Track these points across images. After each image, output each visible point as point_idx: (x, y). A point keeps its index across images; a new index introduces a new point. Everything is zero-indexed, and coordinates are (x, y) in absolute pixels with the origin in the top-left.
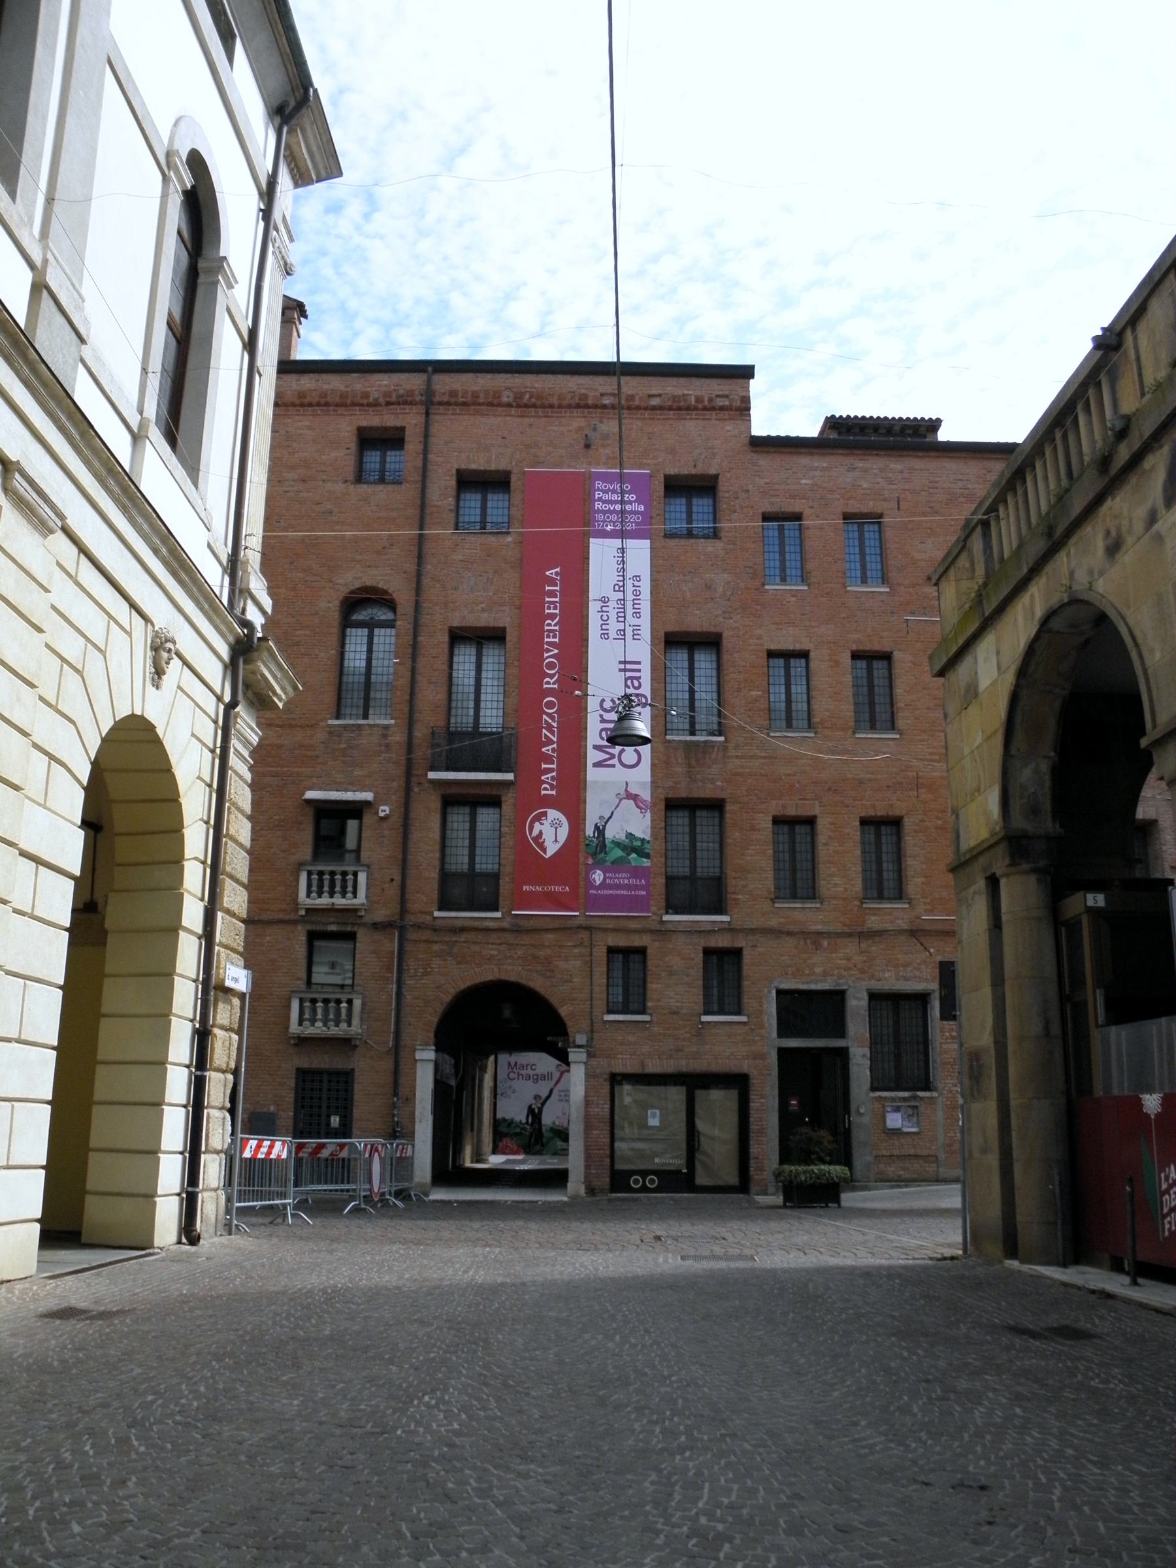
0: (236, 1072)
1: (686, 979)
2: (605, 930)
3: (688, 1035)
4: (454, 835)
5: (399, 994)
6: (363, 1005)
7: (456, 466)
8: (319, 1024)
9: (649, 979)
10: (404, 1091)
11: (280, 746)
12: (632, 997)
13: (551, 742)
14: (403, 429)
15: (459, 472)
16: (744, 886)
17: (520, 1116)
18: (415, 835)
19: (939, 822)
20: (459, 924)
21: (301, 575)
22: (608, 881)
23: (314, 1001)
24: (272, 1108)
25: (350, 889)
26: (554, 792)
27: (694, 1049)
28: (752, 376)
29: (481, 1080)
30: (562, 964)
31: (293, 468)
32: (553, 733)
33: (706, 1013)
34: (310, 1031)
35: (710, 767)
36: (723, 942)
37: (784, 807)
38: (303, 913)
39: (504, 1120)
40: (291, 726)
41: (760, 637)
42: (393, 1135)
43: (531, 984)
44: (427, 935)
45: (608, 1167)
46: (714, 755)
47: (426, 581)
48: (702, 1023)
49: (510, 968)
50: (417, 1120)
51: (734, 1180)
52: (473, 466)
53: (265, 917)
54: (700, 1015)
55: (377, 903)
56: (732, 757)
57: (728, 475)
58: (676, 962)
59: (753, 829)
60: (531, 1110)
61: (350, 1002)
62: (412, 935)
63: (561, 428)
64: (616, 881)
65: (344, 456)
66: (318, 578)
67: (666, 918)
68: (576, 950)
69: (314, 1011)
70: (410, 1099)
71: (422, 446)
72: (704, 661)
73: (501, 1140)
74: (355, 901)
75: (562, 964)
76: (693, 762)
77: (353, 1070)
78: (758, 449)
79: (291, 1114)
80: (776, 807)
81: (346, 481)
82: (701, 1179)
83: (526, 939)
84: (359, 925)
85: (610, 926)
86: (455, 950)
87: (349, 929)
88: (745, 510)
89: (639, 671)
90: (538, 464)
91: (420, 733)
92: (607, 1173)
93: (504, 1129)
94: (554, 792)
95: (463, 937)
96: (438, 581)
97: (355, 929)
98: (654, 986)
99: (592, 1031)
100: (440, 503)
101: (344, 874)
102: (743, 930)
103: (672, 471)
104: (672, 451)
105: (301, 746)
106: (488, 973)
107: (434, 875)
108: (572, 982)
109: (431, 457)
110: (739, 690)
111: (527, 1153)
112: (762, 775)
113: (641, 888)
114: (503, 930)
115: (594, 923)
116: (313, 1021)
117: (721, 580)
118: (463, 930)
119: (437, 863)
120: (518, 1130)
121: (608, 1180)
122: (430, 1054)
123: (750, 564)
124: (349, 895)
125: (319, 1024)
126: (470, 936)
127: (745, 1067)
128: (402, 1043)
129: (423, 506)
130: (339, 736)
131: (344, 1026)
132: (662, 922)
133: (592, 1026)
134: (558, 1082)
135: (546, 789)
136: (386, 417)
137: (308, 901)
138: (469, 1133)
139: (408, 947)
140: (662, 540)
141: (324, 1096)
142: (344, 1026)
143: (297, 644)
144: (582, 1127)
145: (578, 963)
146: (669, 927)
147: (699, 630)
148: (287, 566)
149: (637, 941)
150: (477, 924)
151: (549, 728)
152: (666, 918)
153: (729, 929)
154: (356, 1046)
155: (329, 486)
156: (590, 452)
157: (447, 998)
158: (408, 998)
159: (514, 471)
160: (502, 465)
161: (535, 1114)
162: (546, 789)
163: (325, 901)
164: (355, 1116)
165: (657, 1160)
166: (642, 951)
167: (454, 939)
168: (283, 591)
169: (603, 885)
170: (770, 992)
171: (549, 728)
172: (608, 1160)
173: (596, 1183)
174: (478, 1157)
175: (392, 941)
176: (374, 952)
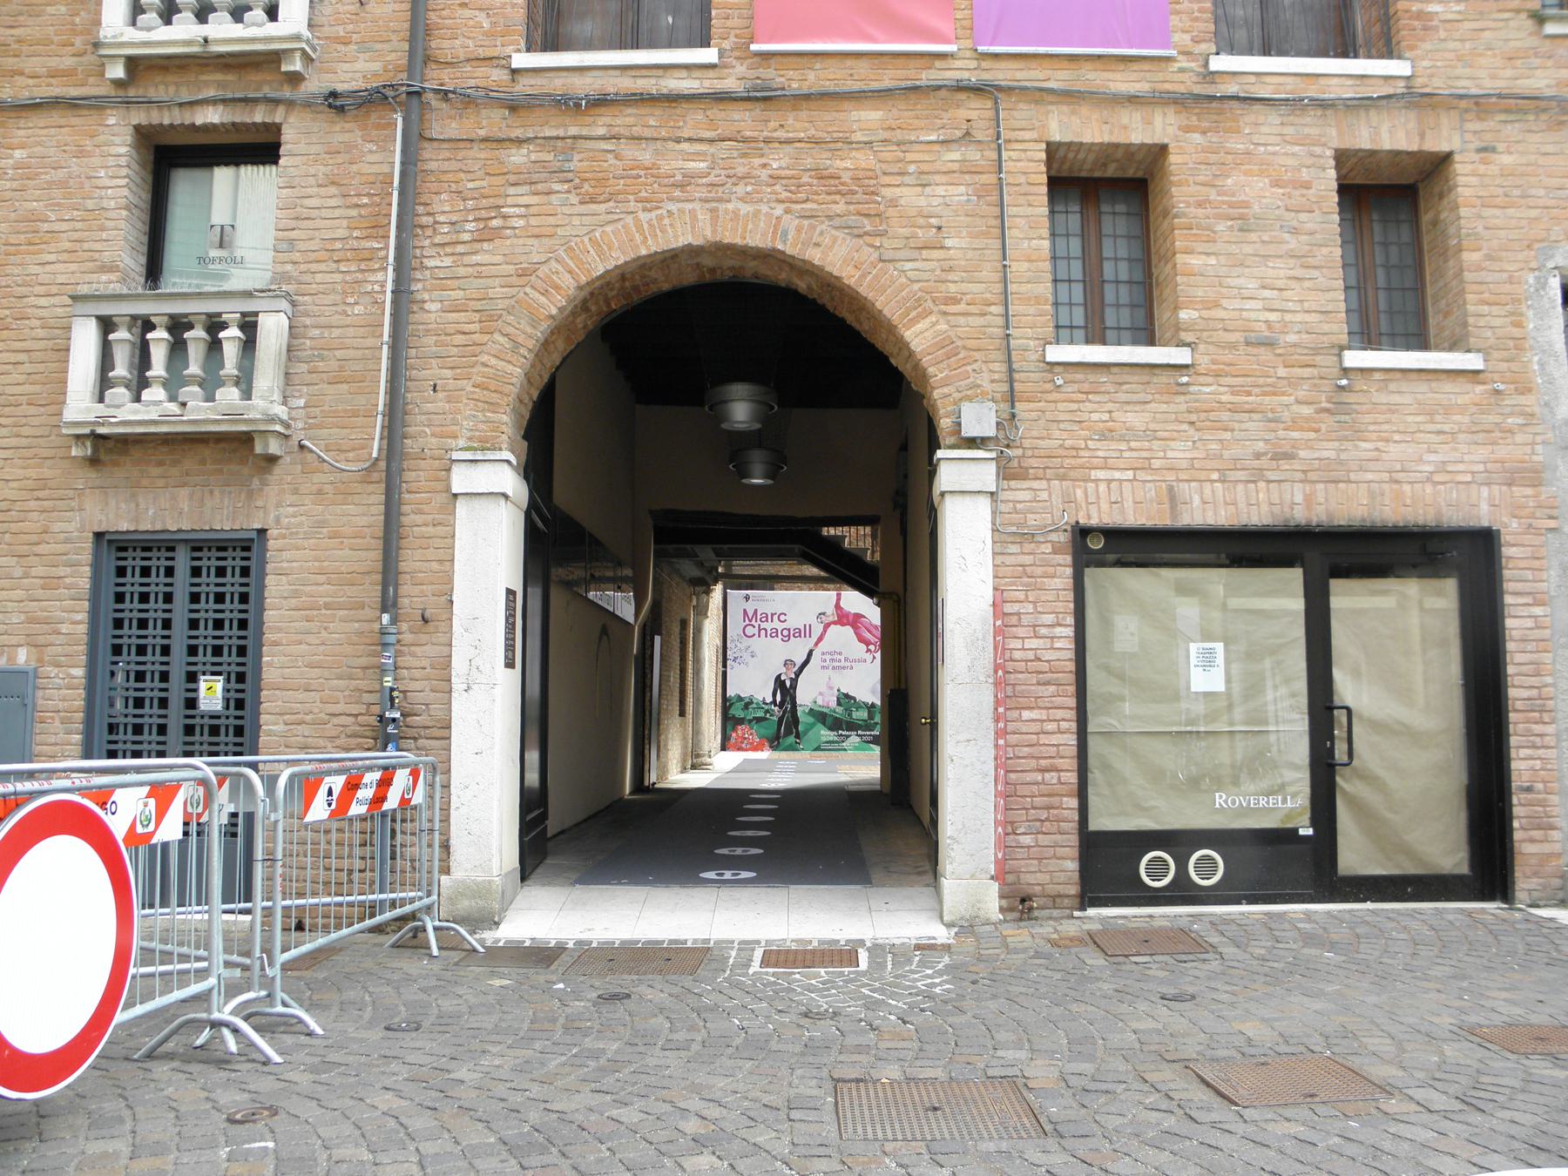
1: (1292, 243)
2: (1040, 95)
3: (1306, 410)
5: (401, 292)
8: (154, 393)
10: (412, 596)
17: (763, 691)
20: (583, 86)
24: (22, 657)
27: (1328, 451)
29: (698, 630)
30: (910, 197)
36: (1392, 135)
38: (118, 71)
39: (740, 698)
42: (384, 733)
43: (815, 256)
44: (493, 121)
45: (1073, 826)
48: (1346, 371)
49: (745, 209)
50: (457, 684)
51: (1447, 851)
54: (1342, 348)
58: (1256, 191)
60: (779, 682)
62: (446, 124)
67: (1220, 63)
69: (143, 358)
70: (434, 620)
73: (734, 729)
74: (271, 29)
75: (910, 197)
77: (262, 532)
79: (79, 672)
82: (1354, 856)
83: (797, 124)
84: (290, 104)
92: (1070, 844)
93: (737, 711)
95: (600, 125)
98: (1195, 261)
99: (1012, 398)
108: (945, 263)
111: (774, 748)
115: (1001, 74)
116: (140, 384)
118: (601, 102)
120: (760, 714)
121: (1072, 866)
126: (624, 120)
131: (229, 395)
132: (1211, 76)
134: (820, 639)
137: (132, 34)
138: (677, 720)
139: (433, 159)
142: (229, 395)
144: (987, 697)
149: (1136, 130)
152: (1220, 63)
153: (1414, 98)
154: (272, 459)
157: (552, 305)
158: (431, 308)
161: (785, 689)
164: (269, 675)
165: (1220, 799)
167: (573, 131)
170: (1542, 285)
172: (1073, 803)
173: (1033, 878)
174: (695, 761)
175: (385, 149)
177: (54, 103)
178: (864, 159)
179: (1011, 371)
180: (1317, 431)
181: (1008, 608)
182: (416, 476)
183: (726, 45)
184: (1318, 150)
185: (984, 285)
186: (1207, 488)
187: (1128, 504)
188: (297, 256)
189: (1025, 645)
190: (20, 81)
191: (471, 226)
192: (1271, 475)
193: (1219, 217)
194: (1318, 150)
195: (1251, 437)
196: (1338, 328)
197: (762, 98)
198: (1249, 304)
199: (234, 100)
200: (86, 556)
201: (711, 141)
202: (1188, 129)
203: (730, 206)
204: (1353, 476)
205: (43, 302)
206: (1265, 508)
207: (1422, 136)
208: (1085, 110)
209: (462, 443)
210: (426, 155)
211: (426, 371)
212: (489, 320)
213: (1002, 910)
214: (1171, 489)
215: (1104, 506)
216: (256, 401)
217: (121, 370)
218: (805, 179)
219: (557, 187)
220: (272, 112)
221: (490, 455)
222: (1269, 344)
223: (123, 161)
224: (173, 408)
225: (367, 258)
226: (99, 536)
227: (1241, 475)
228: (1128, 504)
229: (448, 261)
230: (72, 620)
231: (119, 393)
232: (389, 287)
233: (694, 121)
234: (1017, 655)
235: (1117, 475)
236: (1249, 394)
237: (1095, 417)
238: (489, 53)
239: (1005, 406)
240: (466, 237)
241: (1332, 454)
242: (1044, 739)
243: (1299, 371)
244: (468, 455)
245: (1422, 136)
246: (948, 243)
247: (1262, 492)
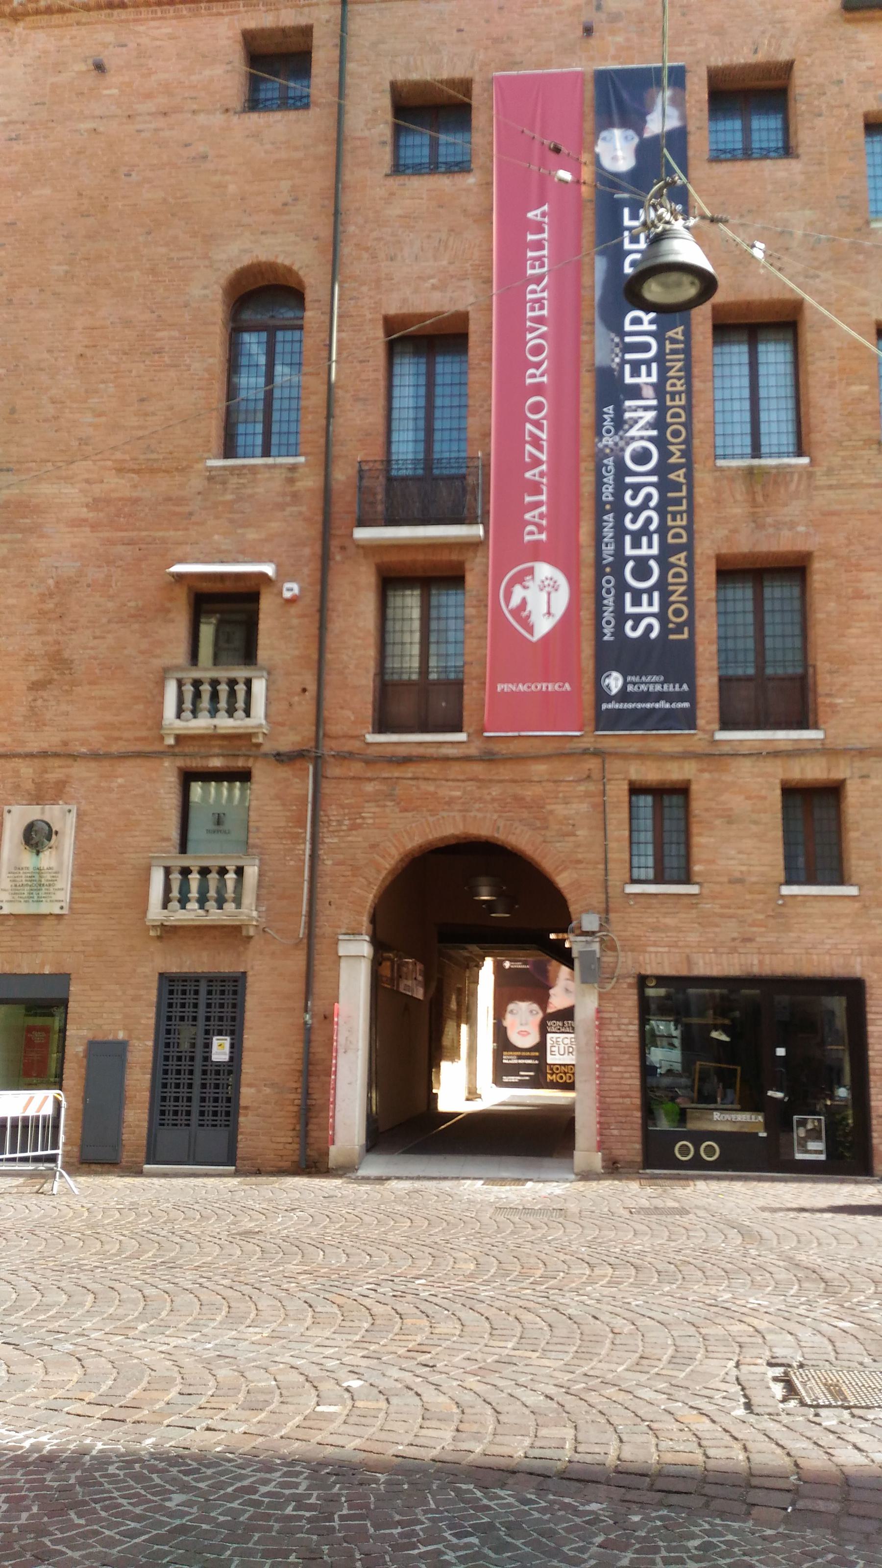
1: (754, 828)
3: (761, 917)
4: (398, 627)
5: (314, 856)
6: (260, 875)
7: (390, 77)
8: (193, 905)
9: (695, 829)
11: (136, 501)
12: (673, 861)
13: (537, 462)
14: (307, 32)
15: (395, 88)
16: (845, 685)
18: (336, 625)
20: (402, 751)
21: (163, 250)
22: (630, 688)
23: (185, 872)
24: (121, 1035)
25: (240, 704)
26: (543, 537)
27: (771, 938)
30: (560, 810)
31: (149, 96)
32: (540, 448)
33: (789, 882)
34: (179, 916)
35: (785, 505)
36: (813, 771)
38: (171, 741)
40: (153, 471)
41: (864, 303)
44: (357, 768)
46: (793, 487)
47: (347, 250)
49: (480, 815)
52: (415, 76)
53: (114, 749)
54: (781, 884)
55: (282, 724)
57: (808, 60)
58: (737, 802)
59: (858, 595)
61: (240, 871)
62: (334, 770)
63: (547, 10)
64: (643, 688)
65: (228, 74)
66: (188, 254)
67: (721, 735)
68: (582, 788)
71: (338, 52)
72: (774, 357)
75: (560, 810)
77: (244, 974)
78: (858, 15)
79: (150, 1043)
81: (227, 110)
83: (505, 772)
84: (256, 757)
85: (632, 750)
86: (398, 791)
87: (240, 763)
88: (836, 112)
90: (514, 65)
91: (343, 474)
94: (543, 537)
95: (410, 771)
96: (367, 249)
97: (250, 763)
99: (607, 911)
100: (366, 133)
101: (232, 683)
102: (845, 751)
103: (719, 60)
104: (719, 31)
105: (169, 499)
106: (449, 826)
107: (366, 681)
109: (351, 66)
110: (831, 385)
112: (871, 513)
113: (680, 697)
114: (467, 759)
116: (183, 901)
118: (407, 760)
119: (371, 666)
121: (638, 1146)
122: (365, 948)
123: (847, 193)
124: (240, 713)
125: (193, 905)
126: (422, 769)
127: (857, 968)
128: (318, 931)
129: (340, 140)
130: (224, 483)
131: (230, 907)
133: (607, 902)
135: (531, 533)
136: (283, 12)
137: (178, 723)
139: (327, 788)
140: (706, 166)
141: (202, 1009)
143: (159, 351)
145: (584, 807)
146: (726, 749)
147: (766, 297)
148: (141, 239)
150: (431, 751)
151: (536, 442)
153: (825, 751)
154: (250, 938)
155: (202, 118)
156: (593, 41)
158: (327, 863)
159: (477, 78)
160: (459, 72)
162: (531, 533)
163: (202, 724)
166: (682, 791)
167: (396, 775)
168: (136, 274)
169: (624, 695)
171: (536, 442)
173: (619, 1152)
175: (304, 779)
176: (277, 797)
177: (139, 755)
178: (538, 790)
179: (607, 898)
180: (765, 927)
181: (606, 1015)
182: (320, 946)
183: (471, 730)
184: (771, 780)
185: (596, 854)
186: (707, 956)
187: (666, 963)
188: (261, 835)
189: (612, 1034)
190: (121, 743)
191: (347, 822)
192: (740, 950)
193: (717, 816)
194: (771, 780)
195: (730, 930)
196: (781, 875)
197: (489, 758)
198: (732, 862)
199: (228, 755)
200: (155, 985)
201: (463, 781)
202: (702, 771)
203: (472, 814)
204: (785, 951)
205: (133, 856)
206: (737, 967)
207: (829, 770)
208: (648, 763)
209: (343, 931)
210: (324, 785)
211: (326, 895)
212: (356, 870)
213: (603, 1167)
214: (688, 957)
215: (654, 965)
216: (243, 910)
217: (175, 893)
218: (509, 800)
219: (389, 803)
220: (247, 760)
221: (358, 937)
222: (740, 881)
223: (172, 785)
224: (201, 912)
225: (297, 838)
226: (161, 975)
227: (725, 950)
228: (666, 963)
229: (336, 840)
230: (148, 1018)
231: (175, 905)
232: (308, 852)
233: (455, 770)
234: (610, 1039)
235: (660, 949)
236: (729, 908)
237: (650, 920)
238: (355, 733)
239: (604, 916)
240: (344, 828)
241: (774, 939)
242: (623, 1081)
243: (756, 897)
244: (347, 937)
245: (829, 770)
246: (578, 833)
247: (735, 959)
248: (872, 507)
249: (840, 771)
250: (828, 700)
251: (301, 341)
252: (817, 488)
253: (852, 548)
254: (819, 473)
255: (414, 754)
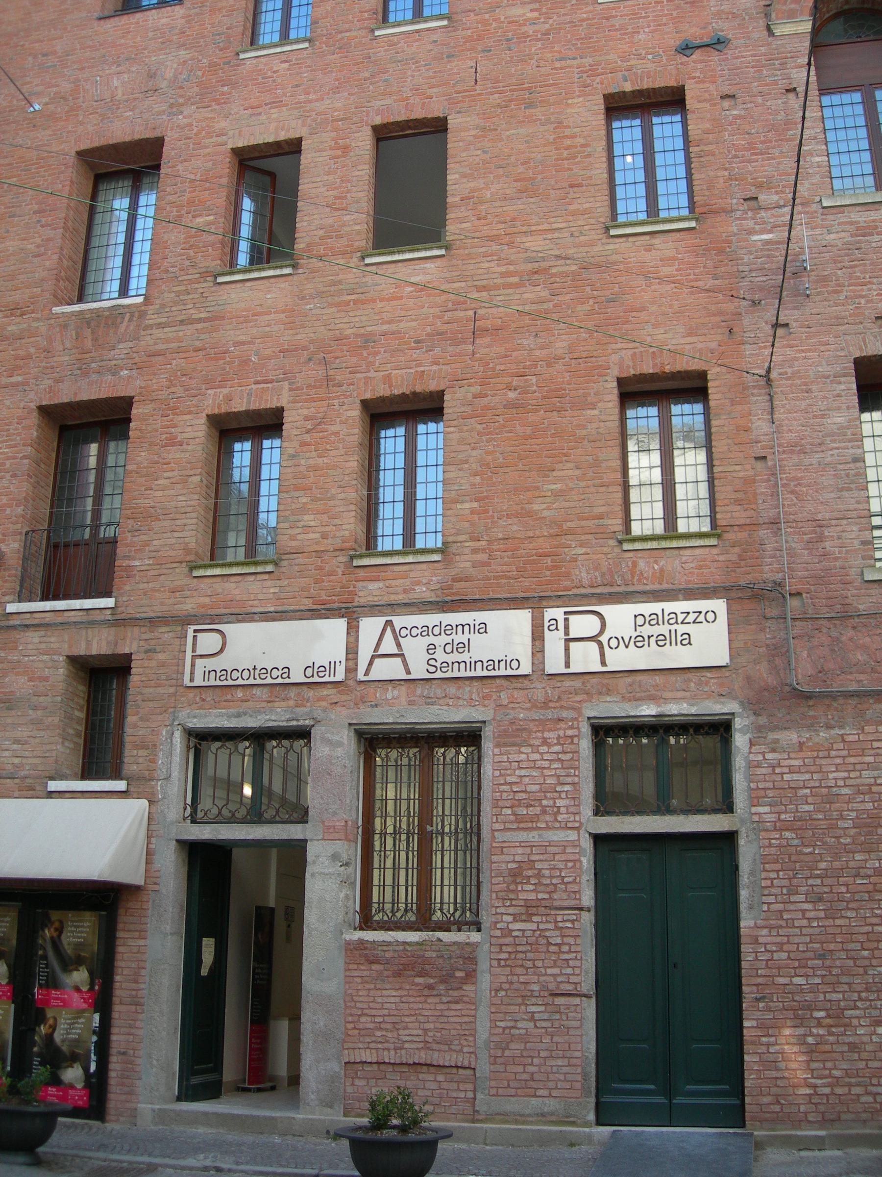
0: (870, 149)
15: (365, 404)
19: (512, 395)
28: (299, 151)
35: (113, 348)
36: (98, 644)
37: (229, 399)
46: (122, 328)
56: (151, 327)
59: (172, 442)
76: (89, 343)
80: (216, 401)
89: (676, 644)
117: (170, 64)
147: (128, 139)
153: (118, 621)
184: (56, 657)
194: (56, 657)
248: (198, 344)
249: (129, 643)
250: (125, 563)
251: (126, 453)
252: (147, 327)
253: (173, 389)
254: (150, 312)
255: (682, 817)
